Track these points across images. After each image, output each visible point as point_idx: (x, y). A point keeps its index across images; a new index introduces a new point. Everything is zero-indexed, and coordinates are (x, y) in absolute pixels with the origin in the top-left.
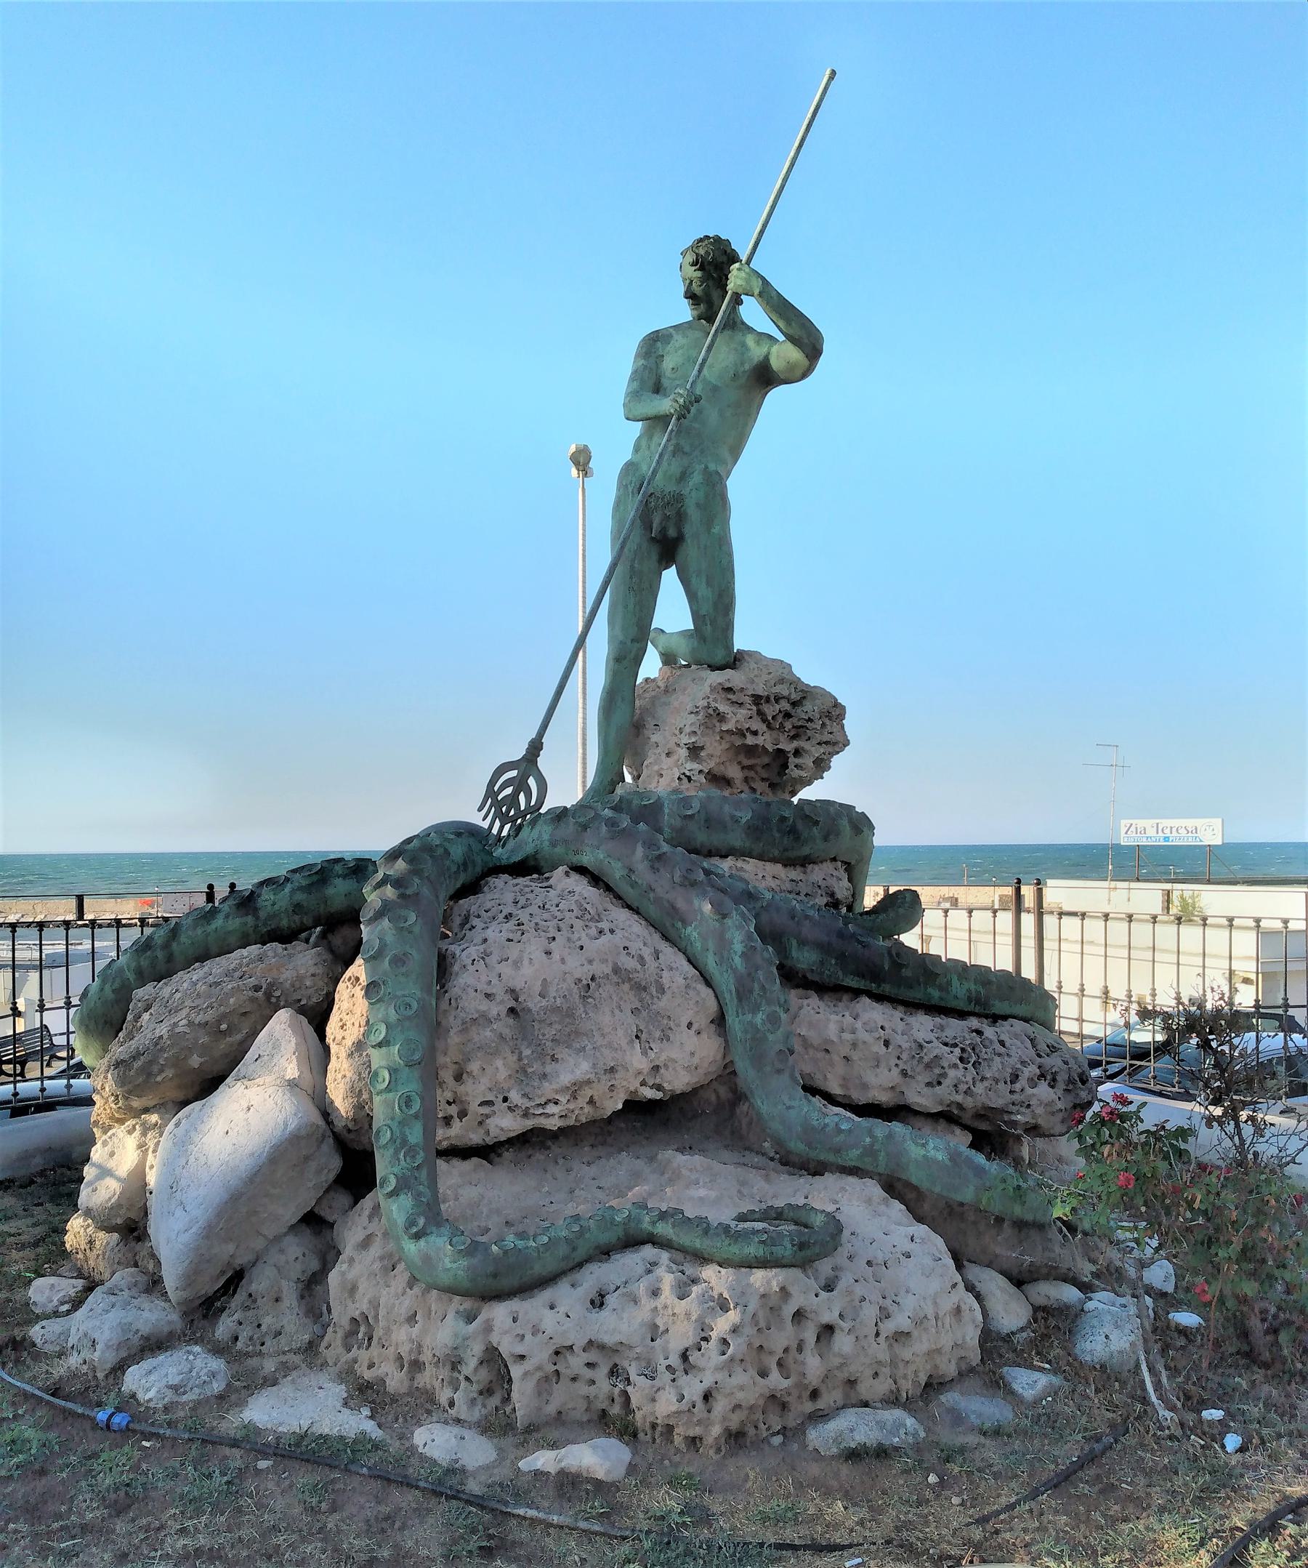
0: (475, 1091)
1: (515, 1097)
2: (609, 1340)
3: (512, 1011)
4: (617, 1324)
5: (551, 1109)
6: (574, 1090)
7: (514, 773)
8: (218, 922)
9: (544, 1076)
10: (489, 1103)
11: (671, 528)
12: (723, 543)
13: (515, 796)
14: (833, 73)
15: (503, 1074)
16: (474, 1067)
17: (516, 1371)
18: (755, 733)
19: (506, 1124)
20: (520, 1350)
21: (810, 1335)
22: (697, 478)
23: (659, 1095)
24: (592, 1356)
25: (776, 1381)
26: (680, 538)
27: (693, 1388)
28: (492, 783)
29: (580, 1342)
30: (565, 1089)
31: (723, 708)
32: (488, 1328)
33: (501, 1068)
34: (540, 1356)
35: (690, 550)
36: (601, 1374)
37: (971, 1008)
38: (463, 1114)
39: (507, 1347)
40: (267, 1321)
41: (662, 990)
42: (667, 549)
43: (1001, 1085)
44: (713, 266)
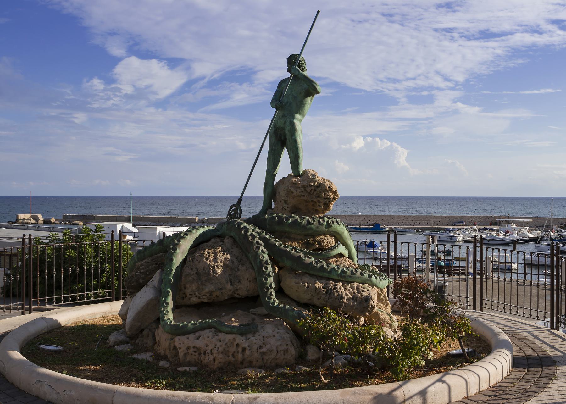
0: (188, 291)
1: (197, 293)
2: (198, 346)
3: (196, 273)
4: (200, 344)
5: (204, 297)
6: (211, 293)
7: (234, 208)
8: (155, 247)
9: (203, 289)
10: (191, 295)
11: (282, 138)
12: (295, 141)
13: (234, 214)
14: (318, 12)
15: (194, 288)
16: (188, 286)
17: (180, 351)
18: (304, 196)
19: (195, 300)
20: (180, 346)
21: (240, 350)
22: (288, 123)
23: (240, 297)
24: (195, 350)
25: (231, 358)
26: (285, 139)
27: (211, 358)
28: (230, 210)
29: (192, 346)
30: (207, 293)
31: (292, 189)
32: (174, 342)
33: (194, 287)
34: (184, 348)
35: (288, 142)
36: (197, 354)
37: (340, 278)
38: (186, 297)
39: (178, 346)
40: (145, 340)
41: (238, 270)
42: (283, 143)
43: (337, 300)
44: (294, 62)
